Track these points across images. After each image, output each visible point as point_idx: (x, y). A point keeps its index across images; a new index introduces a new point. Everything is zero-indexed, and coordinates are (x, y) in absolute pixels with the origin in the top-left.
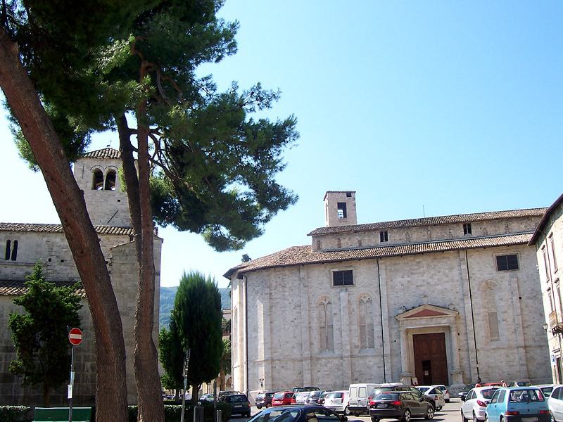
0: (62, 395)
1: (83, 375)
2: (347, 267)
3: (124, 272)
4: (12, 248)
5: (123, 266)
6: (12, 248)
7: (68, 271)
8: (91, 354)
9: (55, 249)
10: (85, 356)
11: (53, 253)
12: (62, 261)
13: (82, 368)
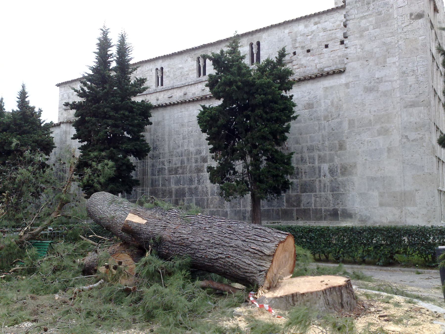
0: (295, 208)
1: (320, 181)
2: (274, 223)
3: (367, 29)
4: (255, 51)
5: (364, 21)
6: (255, 51)
7: (316, 61)
8: (328, 153)
9: (299, 39)
10: (190, 189)
11: (297, 45)
12: (308, 51)
13: (317, 172)
